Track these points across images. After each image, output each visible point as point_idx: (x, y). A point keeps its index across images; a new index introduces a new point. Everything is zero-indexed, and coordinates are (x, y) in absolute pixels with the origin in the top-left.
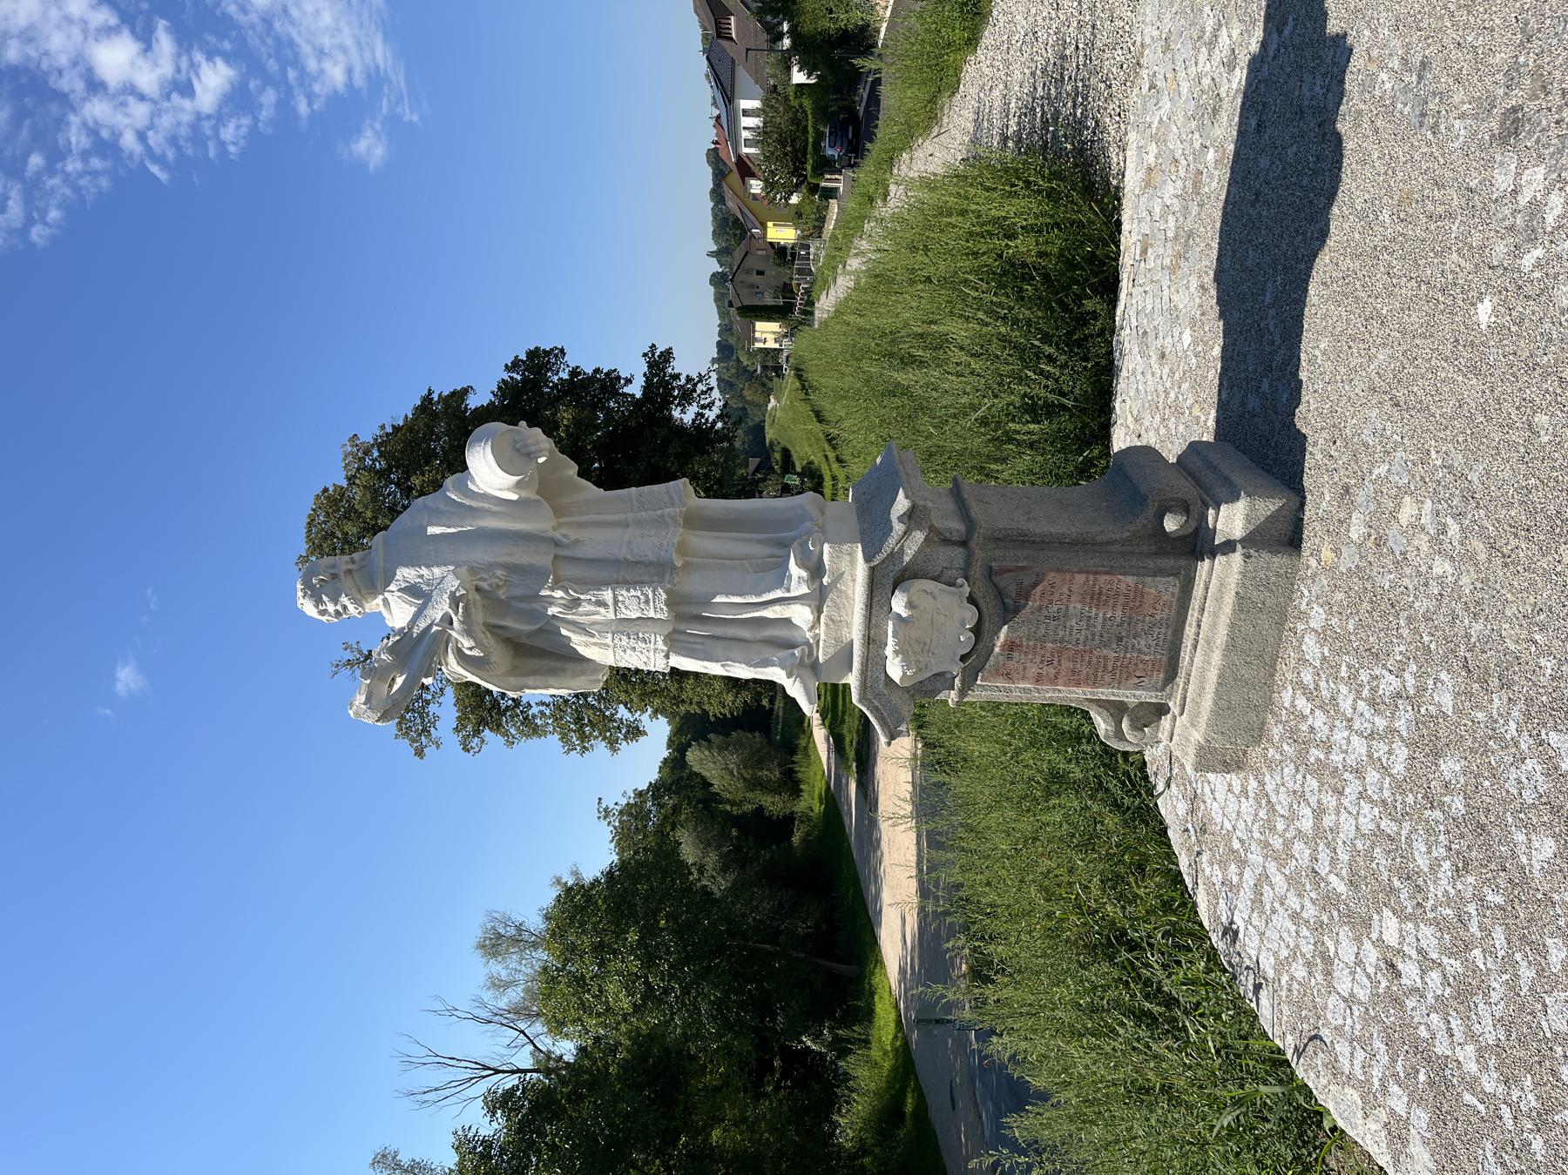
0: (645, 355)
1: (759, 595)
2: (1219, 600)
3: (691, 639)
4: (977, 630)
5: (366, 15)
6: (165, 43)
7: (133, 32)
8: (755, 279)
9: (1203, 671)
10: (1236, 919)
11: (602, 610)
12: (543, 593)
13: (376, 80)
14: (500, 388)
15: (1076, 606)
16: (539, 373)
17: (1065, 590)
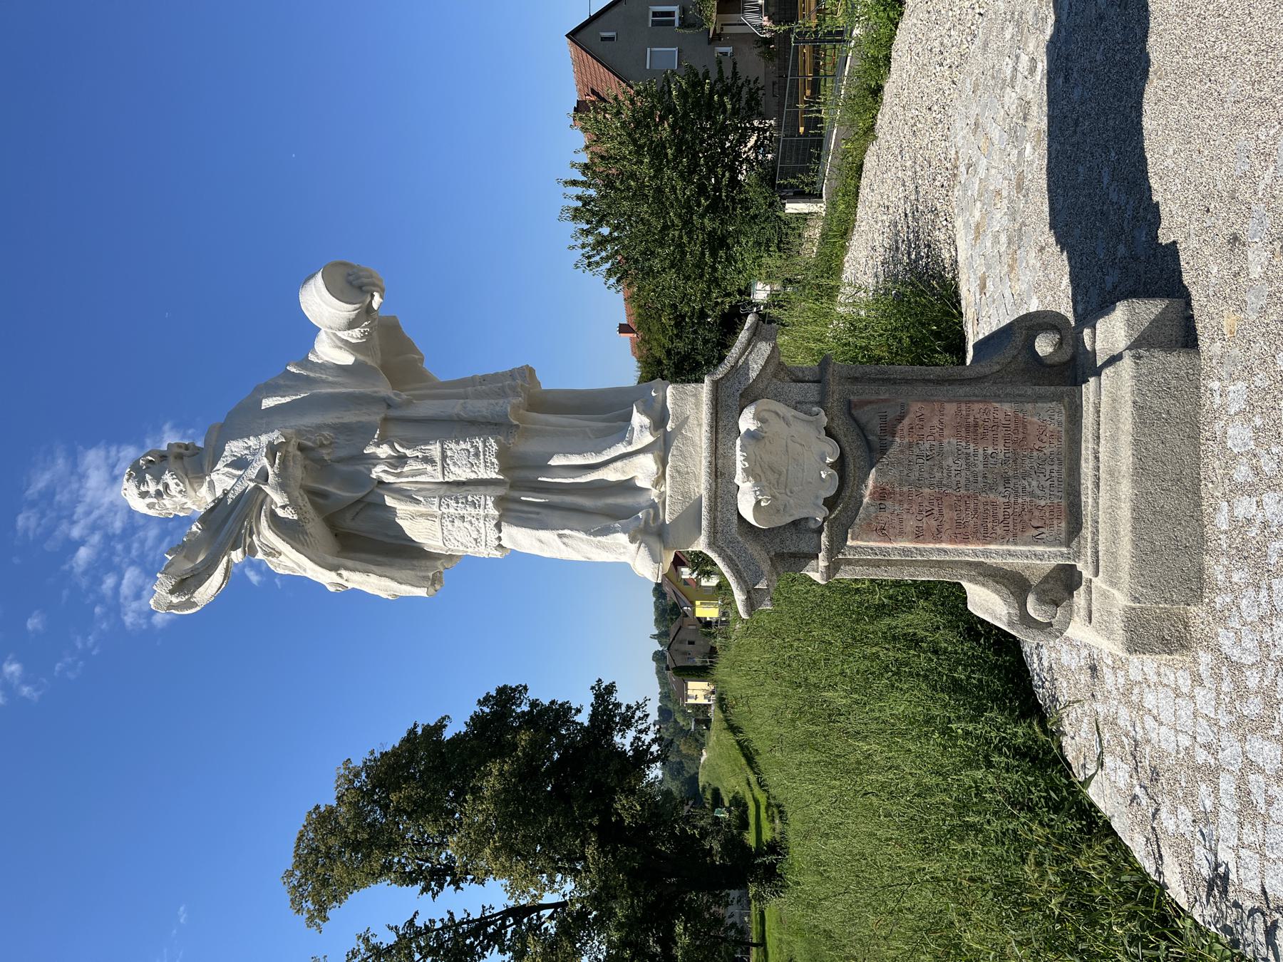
0: (593, 688)
2: (1115, 419)
3: (526, 508)
4: (840, 465)
8: (688, 648)
9: (1113, 509)
10: (1222, 857)
11: (429, 468)
15: (950, 442)
16: (505, 706)
17: (935, 422)
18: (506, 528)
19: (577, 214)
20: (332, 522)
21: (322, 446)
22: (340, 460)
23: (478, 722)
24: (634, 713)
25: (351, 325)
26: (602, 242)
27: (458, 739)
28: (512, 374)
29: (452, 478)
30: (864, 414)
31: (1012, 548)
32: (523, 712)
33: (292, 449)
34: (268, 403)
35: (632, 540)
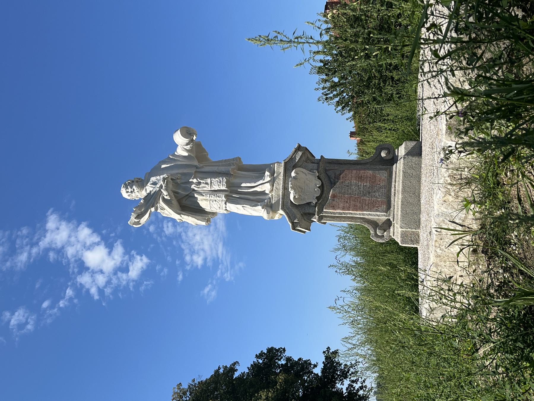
0: (324, 352)
1: (255, 182)
2: (399, 176)
4: (322, 187)
5: (216, 235)
6: (119, 250)
7: (105, 244)
11: (207, 186)
12: (190, 180)
13: (216, 262)
14: (252, 365)
15: (354, 181)
17: (350, 176)
18: (227, 204)
19: (320, 71)
20: (179, 201)
21: (178, 179)
22: (182, 183)
23: (255, 366)
24: (349, 370)
25: (187, 144)
26: (334, 86)
27: (241, 378)
28: (233, 159)
29: (213, 189)
30: (330, 173)
31: (370, 213)
32: (282, 364)
33: (169, 179)
34: (163, 166)
35: (263, 208)
